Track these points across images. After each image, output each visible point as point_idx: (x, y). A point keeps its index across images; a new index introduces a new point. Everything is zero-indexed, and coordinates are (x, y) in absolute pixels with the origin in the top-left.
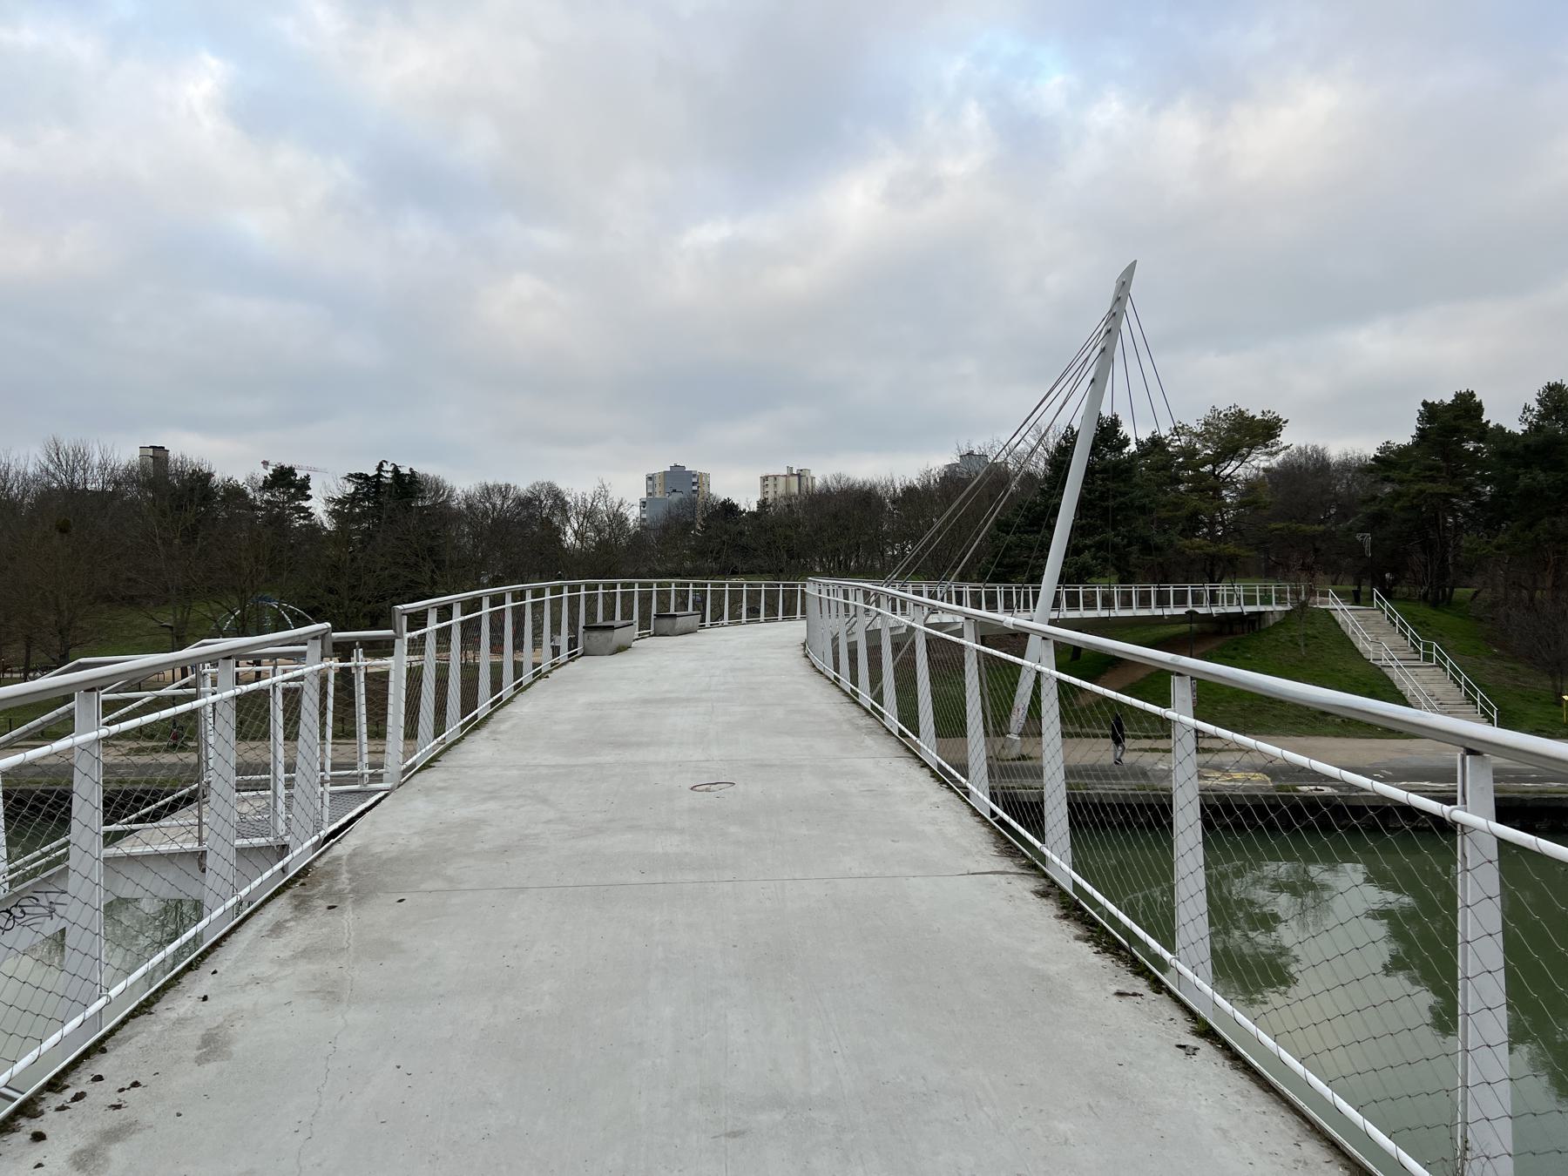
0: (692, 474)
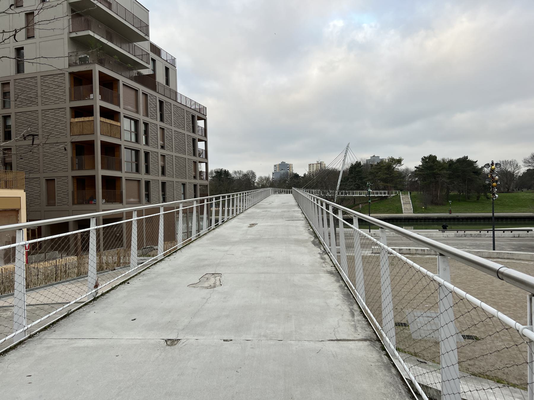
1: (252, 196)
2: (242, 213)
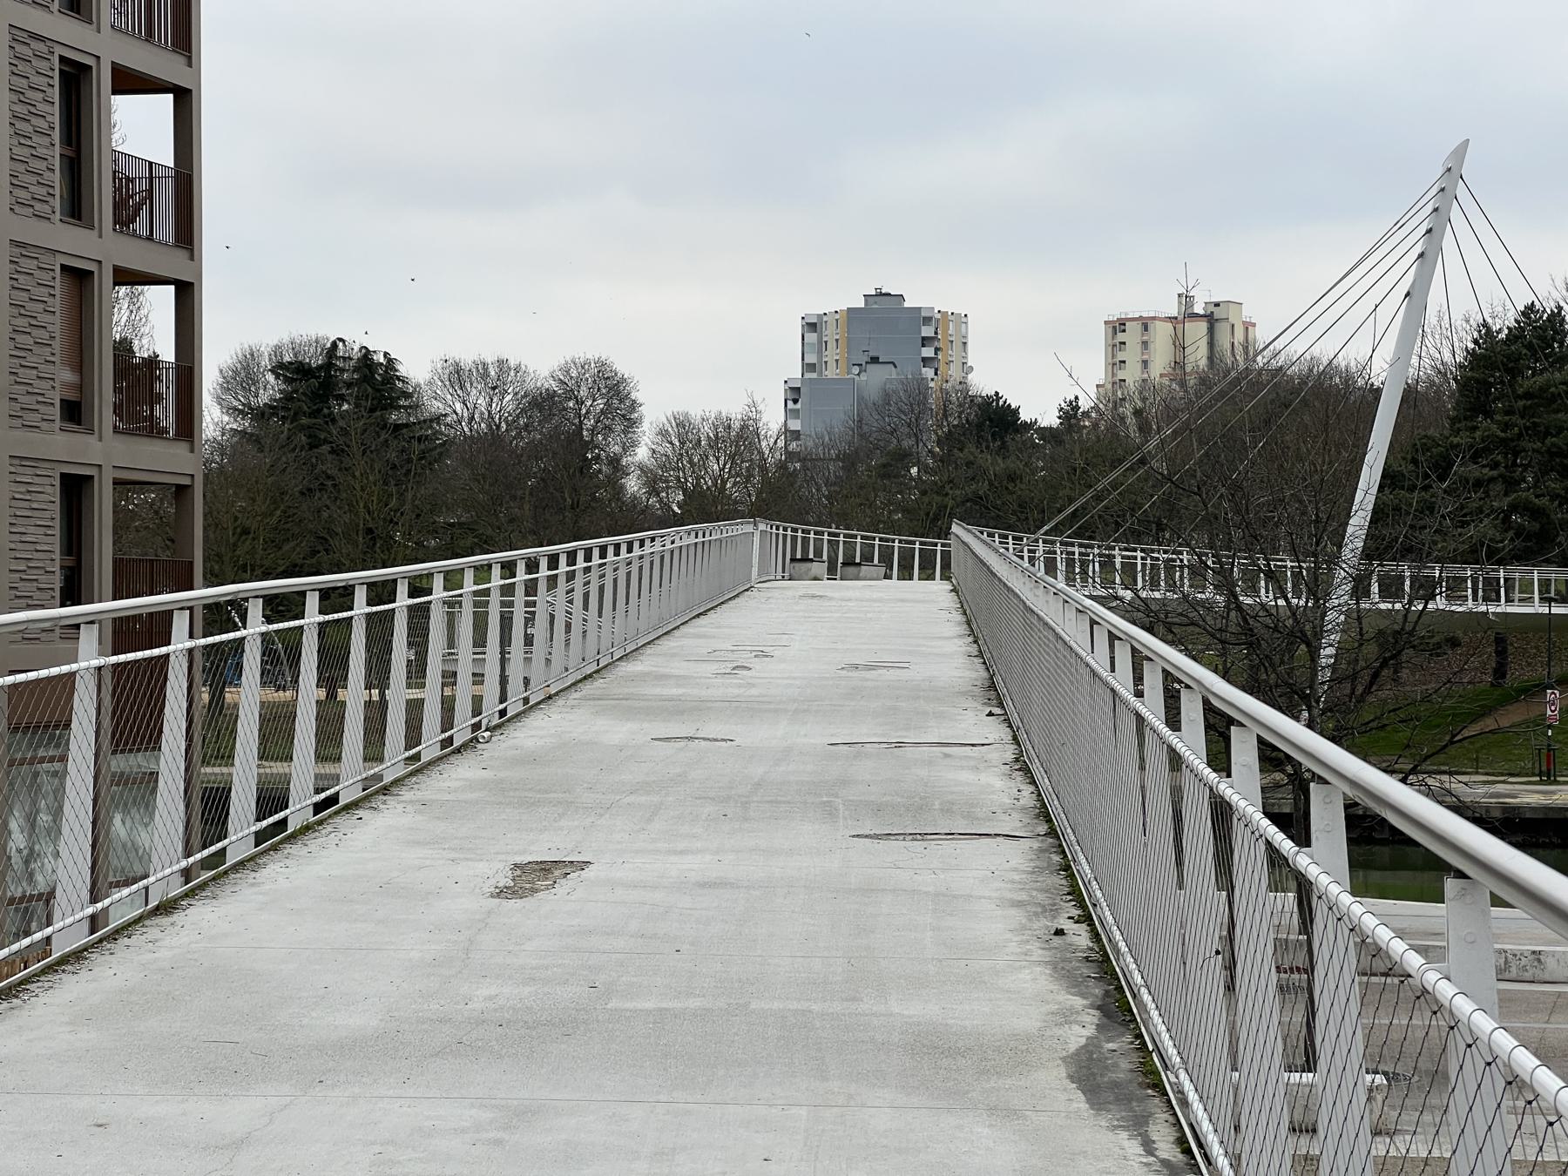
0: (921, 317)
1: (586, 596)
2: (468, 755)
